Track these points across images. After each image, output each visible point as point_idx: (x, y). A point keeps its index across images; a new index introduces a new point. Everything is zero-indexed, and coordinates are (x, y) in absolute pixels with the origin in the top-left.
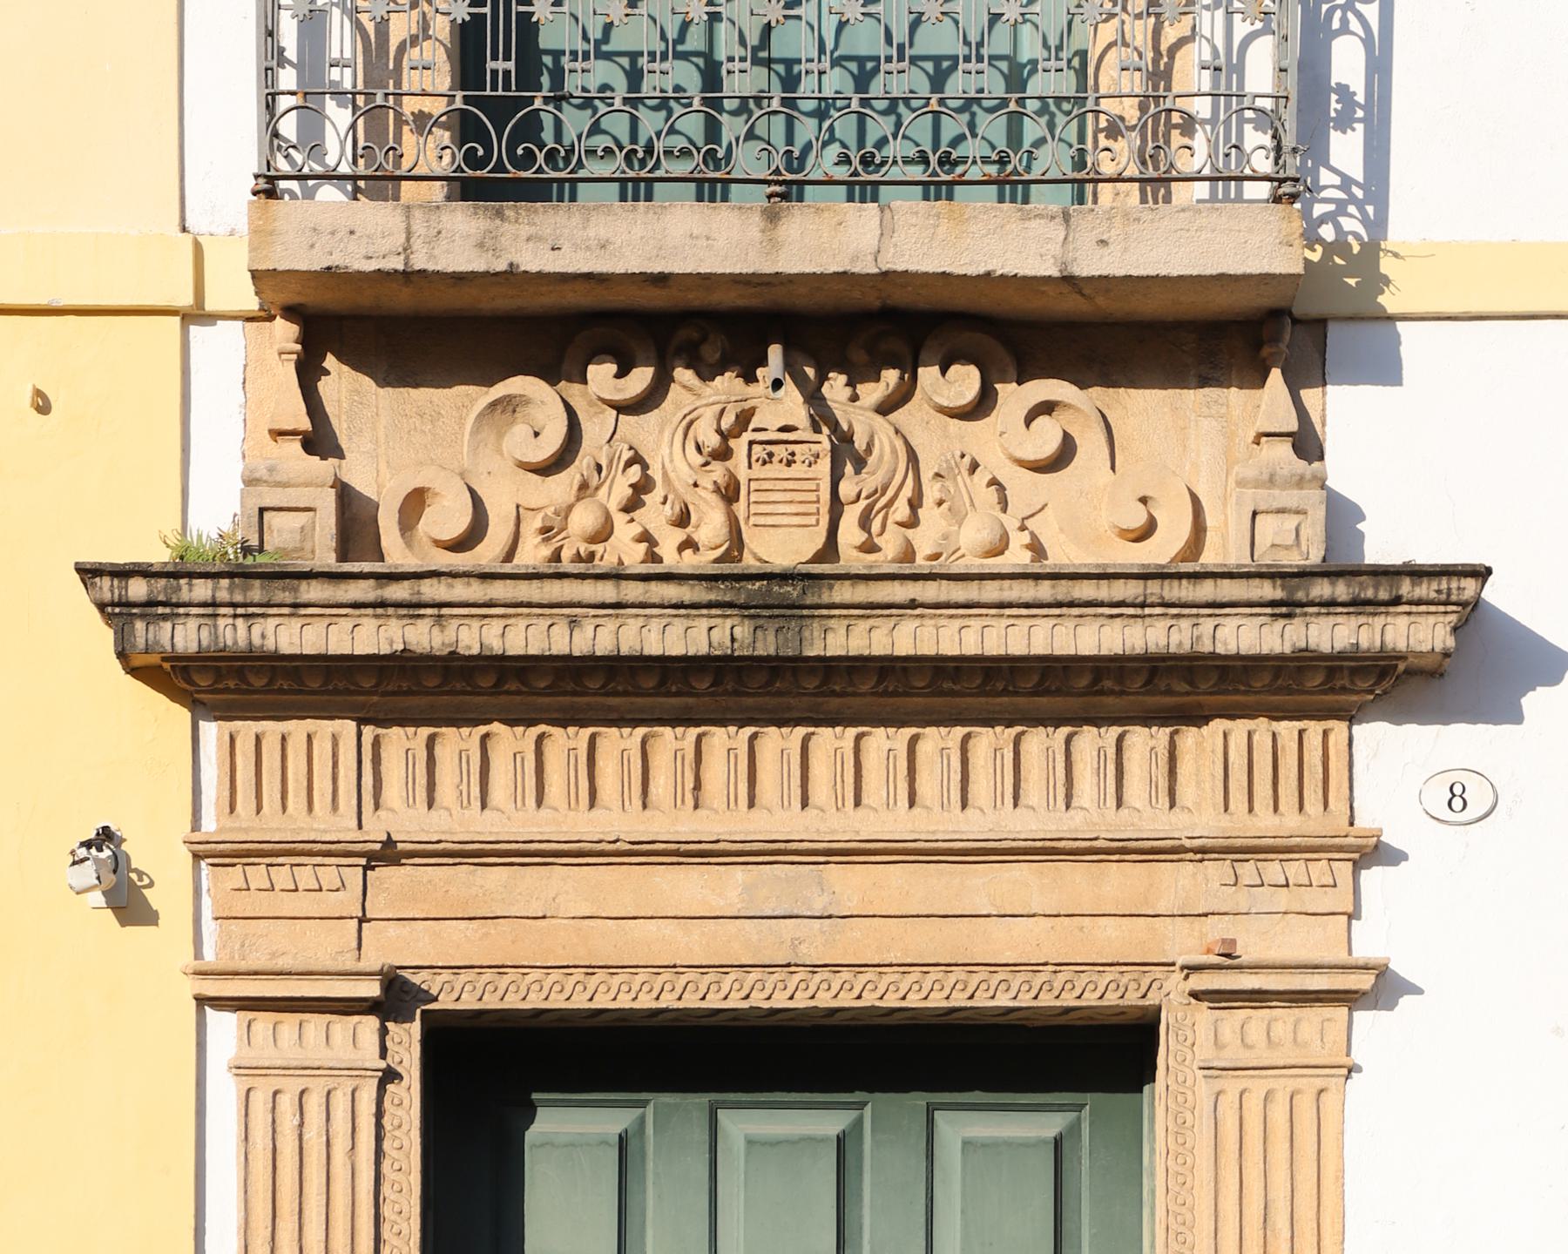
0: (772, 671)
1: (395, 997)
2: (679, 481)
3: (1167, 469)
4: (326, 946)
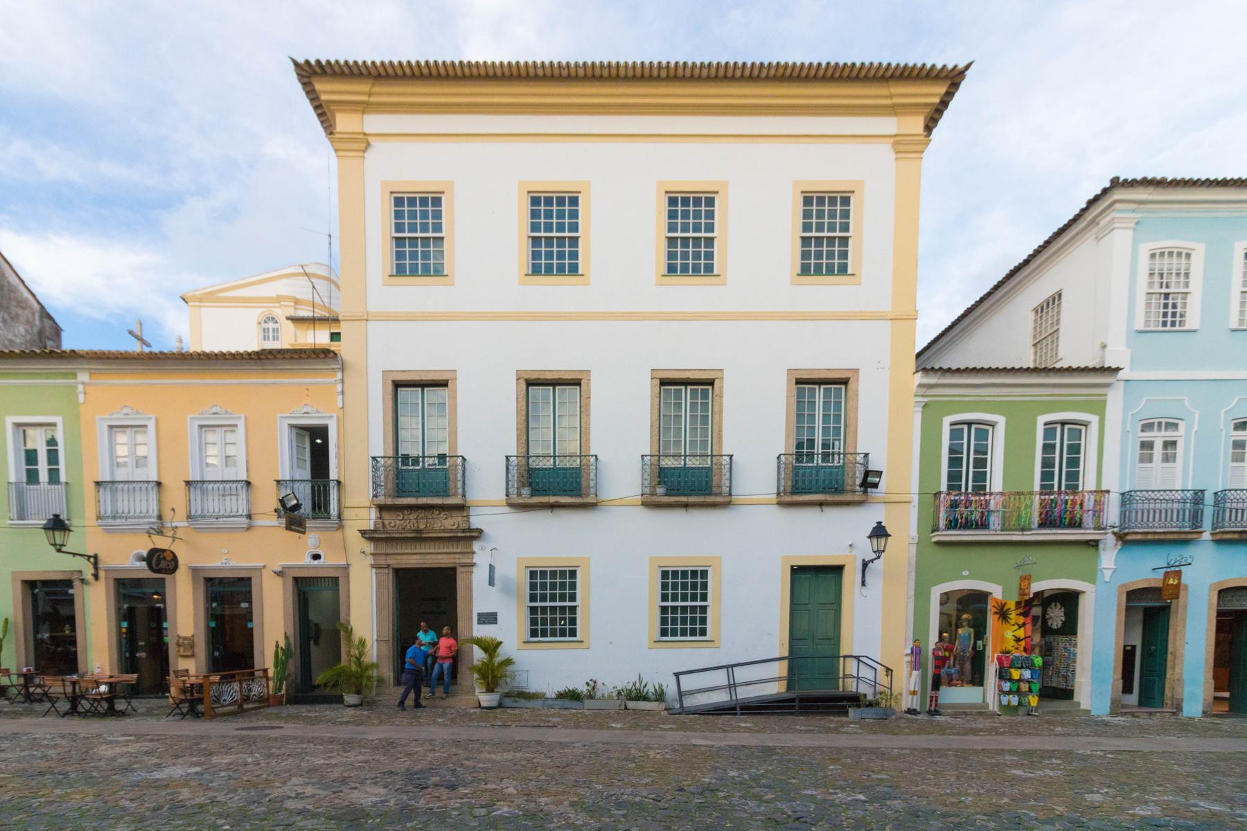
0: (419, 538)
1: (388, 566)
2: (411, 522)
3: (449, 522)
4: (383, 562)
